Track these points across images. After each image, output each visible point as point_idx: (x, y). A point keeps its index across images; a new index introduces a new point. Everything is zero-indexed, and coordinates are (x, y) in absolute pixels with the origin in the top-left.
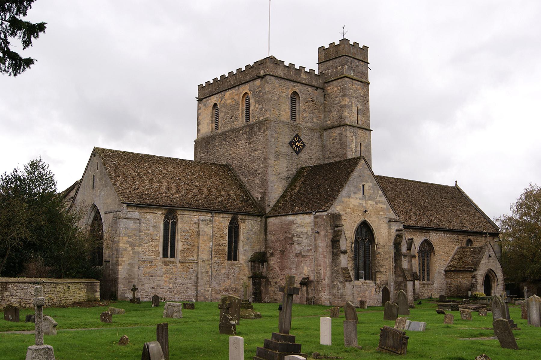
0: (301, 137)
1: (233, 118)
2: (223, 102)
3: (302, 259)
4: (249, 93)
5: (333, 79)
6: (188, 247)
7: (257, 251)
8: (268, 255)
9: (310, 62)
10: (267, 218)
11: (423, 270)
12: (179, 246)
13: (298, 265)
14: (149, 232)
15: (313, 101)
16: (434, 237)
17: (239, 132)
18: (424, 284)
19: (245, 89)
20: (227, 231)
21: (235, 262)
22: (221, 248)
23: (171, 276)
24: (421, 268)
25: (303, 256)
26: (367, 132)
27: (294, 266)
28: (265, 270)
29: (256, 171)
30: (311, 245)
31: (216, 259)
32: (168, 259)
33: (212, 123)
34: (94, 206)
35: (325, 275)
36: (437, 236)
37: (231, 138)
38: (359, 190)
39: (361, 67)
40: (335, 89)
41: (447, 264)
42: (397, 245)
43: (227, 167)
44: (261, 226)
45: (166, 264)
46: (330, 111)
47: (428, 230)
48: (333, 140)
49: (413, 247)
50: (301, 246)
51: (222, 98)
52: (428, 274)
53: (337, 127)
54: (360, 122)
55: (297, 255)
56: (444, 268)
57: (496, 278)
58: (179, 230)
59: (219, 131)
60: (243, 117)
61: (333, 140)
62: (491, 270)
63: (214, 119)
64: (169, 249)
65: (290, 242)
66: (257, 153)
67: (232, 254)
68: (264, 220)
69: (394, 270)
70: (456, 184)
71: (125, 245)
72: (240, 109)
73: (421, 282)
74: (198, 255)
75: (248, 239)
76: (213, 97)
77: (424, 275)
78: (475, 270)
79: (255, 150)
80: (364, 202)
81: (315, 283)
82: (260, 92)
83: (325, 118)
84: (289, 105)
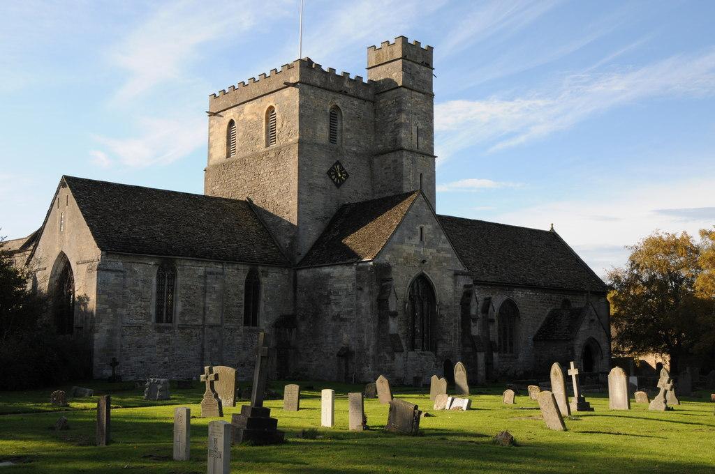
2: (241, 118)
16: (519, 296)
19: (269, 101)
20: (243, 287)
23: (167, 347)
25: (342, 320)
26: (420, 159)
34: (62, 256)
38: (415, 234)
40: (389, 103)
45: (160, 330)
47: (511, 286)
49: (491, 308)
52: (511, 344)
53: (391, 152)
55: (334, 318)
56: (532, 337)
58: (179, 286)
67: (251, 317)
70: (552, 229)
71: (104, 306)
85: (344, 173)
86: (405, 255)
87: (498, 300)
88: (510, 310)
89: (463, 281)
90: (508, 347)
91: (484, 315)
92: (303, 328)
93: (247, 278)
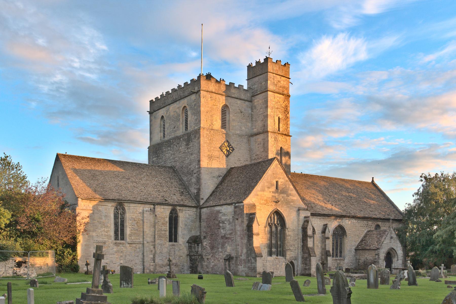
0: (231, 143)
1: (175, 128)
2: (168, 115)
3: (226, 241)
4: (187, 106)
5: (259, 93)
6: (135, 232)
7: (194, 235)
8: (202, 237)
9: (228, 84)
10: (201, 208)
11: (337, 249)
12: (128, 231)
13: (223, 246)
14: (101, 220)
15: (241, 112)
16: (347, 223)
17: (180, 139)
18: (336, 260)
19: (184, 102)
20: (167, 219)
21: (175, 243)
22: (163, 232)
23: (122, 254)
24: (335, 248)
25: (227, 238)
27: (220, 246)
28: (200, 249)
29: (193, 171)
30: (232, 229)
31: (159, 241)
32: (339, 258)
33: (160, 132)
35: (242, 253)
36: (350, 222)
37: (175, 145)
38: (272, 185)
39: (282, 82)
41: (357, 244)
42: (304, 229)
43: (172, 168)
44: (196, 215)
46: (256, 121)
47: (341, 217)
48: (258, 144)
49: (327, 230)
50: (225, 230)
51: (167, 111)
52: (341, 252)
53: (261, 133)
54: (281, 130)
55: (222, 237)
56: (354, 248)
57: (396, 255)
58: (127, 219)
59: (166, 139)
60: (183, 126)
61: (258, 144)
62: (392, 248)
63: (162, 129)
64: (120, 233)
65: (217, 227)
66: (193, 156)
68: (199, 210)
69: (302, 248)
70: (373, 181)
72: (181, 120)
73: (334, 258)
74: (144, 238)
75: (186, 225)
76: (160, 111)
77: (337, 253)
78: (378, 249)
79: (192, 154)
80: (277, 195)
81: (235, 259)
82: (195, 105)
83: (252, 126)
84: (220, 116)
85: (231, 148)
86: (265, 198)
87: (333, 224)
88: (340, 232)
89: (303, 214)
90: (339, 254)
91: (323, 234)
92: (205, 244)
93: (170, 214)
